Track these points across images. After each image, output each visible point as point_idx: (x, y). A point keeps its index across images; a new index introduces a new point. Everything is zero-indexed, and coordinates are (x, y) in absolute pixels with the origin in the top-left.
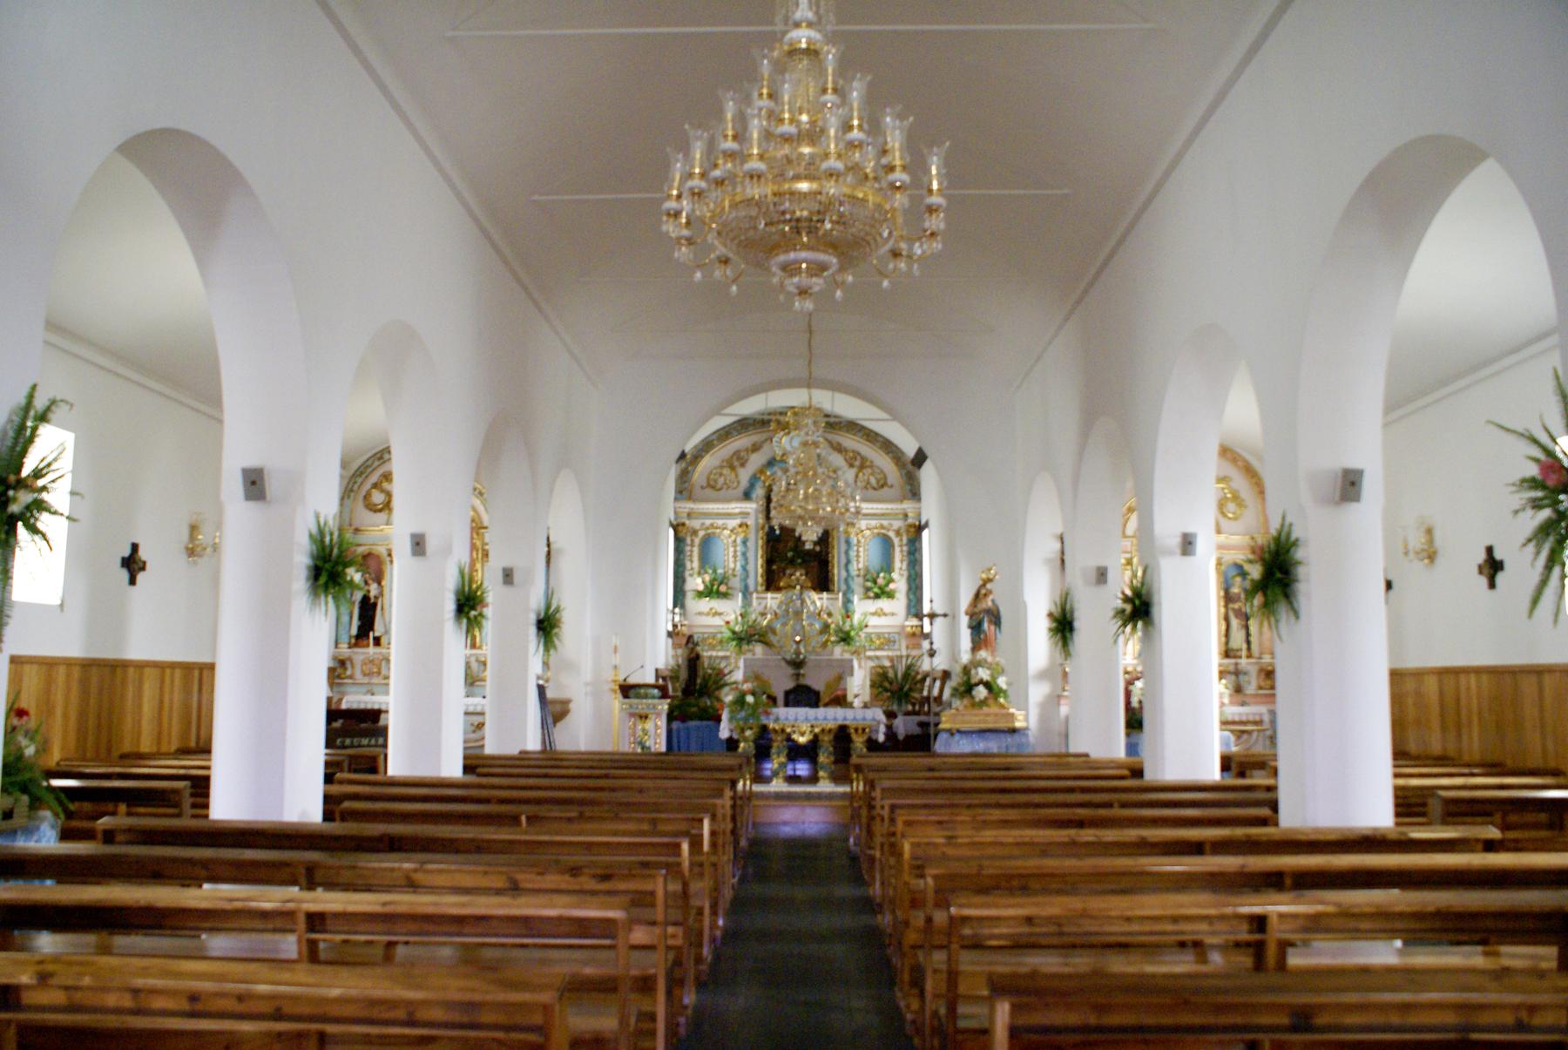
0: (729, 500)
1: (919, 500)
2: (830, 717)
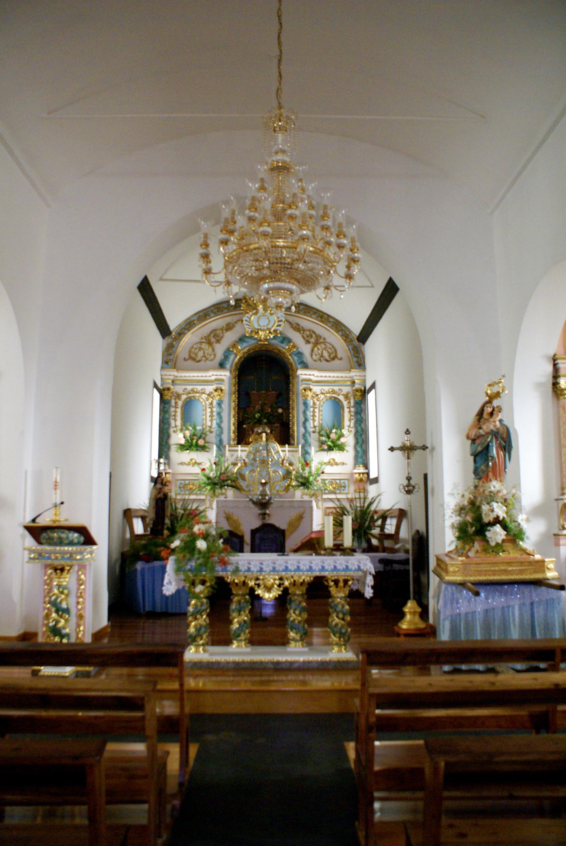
0: (207, 369)
1: (364, 369)
2: (304, 566)
